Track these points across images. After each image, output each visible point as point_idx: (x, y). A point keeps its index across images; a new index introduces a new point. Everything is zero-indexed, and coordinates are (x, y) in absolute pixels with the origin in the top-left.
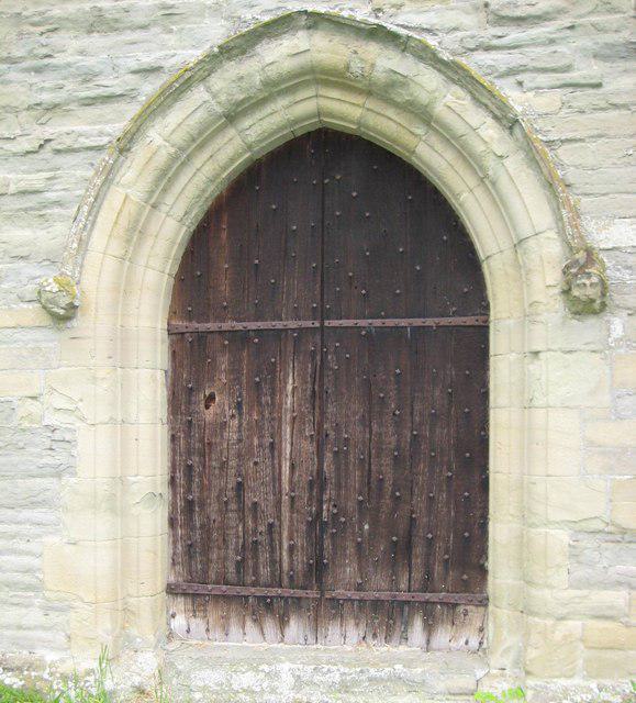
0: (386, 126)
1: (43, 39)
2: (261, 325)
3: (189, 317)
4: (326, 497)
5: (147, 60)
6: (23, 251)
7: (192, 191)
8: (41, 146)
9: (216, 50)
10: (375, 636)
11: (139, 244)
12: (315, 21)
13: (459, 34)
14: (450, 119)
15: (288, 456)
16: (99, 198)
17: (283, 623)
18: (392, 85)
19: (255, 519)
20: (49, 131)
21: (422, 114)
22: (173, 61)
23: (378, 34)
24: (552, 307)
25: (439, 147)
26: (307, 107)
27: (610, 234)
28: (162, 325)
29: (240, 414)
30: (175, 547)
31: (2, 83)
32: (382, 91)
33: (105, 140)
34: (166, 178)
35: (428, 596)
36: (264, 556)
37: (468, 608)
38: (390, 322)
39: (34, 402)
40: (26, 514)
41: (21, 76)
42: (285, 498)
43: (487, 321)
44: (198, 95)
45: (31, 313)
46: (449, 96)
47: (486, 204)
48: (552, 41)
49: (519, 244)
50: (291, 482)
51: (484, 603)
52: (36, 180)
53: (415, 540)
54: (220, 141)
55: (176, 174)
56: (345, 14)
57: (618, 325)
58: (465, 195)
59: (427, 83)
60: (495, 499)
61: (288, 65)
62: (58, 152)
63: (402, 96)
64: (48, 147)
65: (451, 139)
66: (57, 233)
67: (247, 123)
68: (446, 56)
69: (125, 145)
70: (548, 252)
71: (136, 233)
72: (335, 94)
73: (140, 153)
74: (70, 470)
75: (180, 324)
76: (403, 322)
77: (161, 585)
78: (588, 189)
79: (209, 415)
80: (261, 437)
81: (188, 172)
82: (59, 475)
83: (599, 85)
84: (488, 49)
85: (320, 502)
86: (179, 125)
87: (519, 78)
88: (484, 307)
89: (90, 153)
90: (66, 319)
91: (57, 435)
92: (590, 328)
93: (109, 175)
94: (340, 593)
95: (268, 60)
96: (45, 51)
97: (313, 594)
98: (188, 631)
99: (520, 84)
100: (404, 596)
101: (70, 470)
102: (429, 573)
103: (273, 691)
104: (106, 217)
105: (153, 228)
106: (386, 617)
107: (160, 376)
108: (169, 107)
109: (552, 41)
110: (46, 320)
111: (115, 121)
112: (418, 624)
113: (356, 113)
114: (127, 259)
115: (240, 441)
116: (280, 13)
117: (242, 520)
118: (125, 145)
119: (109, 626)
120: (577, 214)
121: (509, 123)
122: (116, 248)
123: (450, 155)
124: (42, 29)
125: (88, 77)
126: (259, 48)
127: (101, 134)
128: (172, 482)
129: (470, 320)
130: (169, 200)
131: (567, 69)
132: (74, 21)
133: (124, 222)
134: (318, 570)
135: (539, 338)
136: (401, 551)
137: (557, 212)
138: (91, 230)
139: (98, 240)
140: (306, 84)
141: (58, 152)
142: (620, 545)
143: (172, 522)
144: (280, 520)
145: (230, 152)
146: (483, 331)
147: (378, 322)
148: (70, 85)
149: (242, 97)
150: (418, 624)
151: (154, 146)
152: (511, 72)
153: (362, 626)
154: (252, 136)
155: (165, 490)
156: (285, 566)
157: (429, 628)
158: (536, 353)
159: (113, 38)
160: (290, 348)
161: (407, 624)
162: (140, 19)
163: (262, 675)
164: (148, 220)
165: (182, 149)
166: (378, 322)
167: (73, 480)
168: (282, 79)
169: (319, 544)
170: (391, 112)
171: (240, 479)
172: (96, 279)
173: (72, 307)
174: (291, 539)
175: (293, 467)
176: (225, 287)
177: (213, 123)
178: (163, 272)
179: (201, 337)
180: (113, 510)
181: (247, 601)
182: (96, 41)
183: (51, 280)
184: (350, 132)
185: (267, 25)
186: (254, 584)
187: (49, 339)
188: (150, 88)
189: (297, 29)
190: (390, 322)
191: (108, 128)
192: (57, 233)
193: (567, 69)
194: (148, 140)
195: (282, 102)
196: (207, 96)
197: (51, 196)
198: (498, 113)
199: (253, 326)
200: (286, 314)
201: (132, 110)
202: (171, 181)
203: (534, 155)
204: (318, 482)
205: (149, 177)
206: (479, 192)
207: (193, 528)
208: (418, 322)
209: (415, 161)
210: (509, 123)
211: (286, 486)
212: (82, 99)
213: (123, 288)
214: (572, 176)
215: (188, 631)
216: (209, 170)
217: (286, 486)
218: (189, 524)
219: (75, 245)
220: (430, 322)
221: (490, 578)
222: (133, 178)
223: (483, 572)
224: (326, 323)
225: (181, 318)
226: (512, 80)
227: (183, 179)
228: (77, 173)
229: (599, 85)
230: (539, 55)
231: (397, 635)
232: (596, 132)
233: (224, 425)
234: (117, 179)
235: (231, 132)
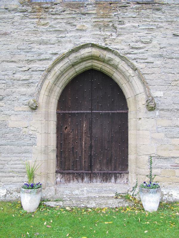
0: (107, 69)
1: (29, 45)
2: (79, 112)
3: (61, 109)
4: (92, 150)
5: (54, 52)
6: (24, 93)
7: (63, 81)
8: (28, 69)
9: (71, 50)
10: (104, 181)
11: (51, 93)
12: (93, 45)
13: (124, 50)
14: (122, 68)
15: (84, 141)
16: (43, 82)
17: (83, 179)
18: (109, 60)
19: (76, 155)
20: (30, 66)
21: (116, 67)
22: (60, 52)
23: (106, 49)
24: (144, 109)
25: (118, 74)
26: (90, 64)
27: (157, 94)
28: (55, 111)
29: (73, 131)
30: (57, 162)
31: (178, 110)
32: (107, 62)
33: (45, 69)
34: (58, 78)
35: (115, 172)
36: (78, 164)
37: (124, 174)
38: (107, 112)
39: (26, 129)
40: (24, 155)
41: (24, 53)
42: (83, 150)
43: (128, 112)
44: (66, 60)
45: (27, 108)
46: (122, 63)
47: (128, 87)
48: (143, 53)
50: (85, 146)
52: (27, 77)
53: (113, 159)
54: (70, 71)
55: (60, 77)
56: (100, 44)
58: (123, 85)
59: (117, 60)
60: (137, 153)
61: (87, 55)
62: (33, 71)
63: (112, 63)
64: (30, 70)
65: (121, 72)
66: (33, 89)
67: (76, 67)
68: (121, 55)
69: (49, 71)
71: (51, 91)
72: (96, 62)
73: (53, 73)
74: (35, 144)
75: (60, 112)
76: (110, 112)
77: (55, 171)
78: (151, 84)
79: (66, 132)
80: (78, 136)
81: (63, 77)
82: (32, 146)
83: (153, 63)
84: (130, 54)
85: (91, 151)
86: (62, 67)
87: (137, 60)
88: (127, 109)
89: (40, 72)
90: (35, 109)
91: (32, 136)
92: (151, 114)
93: (45, 77)
94: (96, 171)
95: (82, 53)
96: (30, 48)
97: (90, 172)
98: (61, 181)
99: (137, 61)
100: (111, 172)
101: (35, 144)
102: (115, 167)
103: (83, 194)
104: (45, 86)
105: (55, 90)
106: (106, 177)
107: (55, 123)
108: (60, 62)
109: (143, 53)
110: (29, 109)
112: (113, 178)
113: (100, 66)
114: (49, 96)
115: (73, 137)
116: (85, 43)
117: (74, 155)
118: (49, 71)
119: (44, 181)
120: (149, 89)
121: (135, 69)
122: (46, 94)
123: (121, 76)
124: (29, 43)
125: (40, 54)
126: (80, 51)
127: (43, 67)
128: (57, 147)
129: (124, 112)
130: (59, 83)
131: (146, 59)
132: (36, 41)
133: (49, 87)
134: (91, 167)
135: (141, 115)
136: (109, 162)
137: (145, 88)
138: (41, 89)
139: (43, 92)
140: (90, 59)
141: (33, 71)
142: (158, 159)
143: (57, 156)
144: (82, 155)
146: (127, 114)
147: (104, 112)
148: (35, 56)
149: (76, 61)
150: (113, 178)
151: (56, 71)
152: (135, 59)
153: (101, 179)
154: (77, 70)
155: (55, 148)
156: (83, 165)
157: (116, 179)
158: (140, 119)
159: (45, 46)
160: (84, 117)
161: (111, 178)
162: (52, 42)
163: (79, 191)
164: (53, 88)
165: (62, 72)
166: (104, 112)
167: (36, 146)
168: (85, 58)
169: (91, 161)
170: (108, 66)
171: (73, 146)
172: (42, 100)
173: (37, 106)
174: (85, 159)
175: (85, 143)
176: (70, 103)
177: (70, 66)
179: (64, 114)
180: (45, 154)
181: (74, 174)
182: (42, 47)
183: (32, 100)
184: (98, 70)
185: (82, 46)
186: (76, 170)
188: (55, 58)
189: (89, 47)
190: (107, 112)
191: (45, 66)
192: (33, 89)
193: (146, 59)
194: (55, 69)
195: (84, 63)
196: (68, 60)
197: (31, 81)
198: (132, 67)
199: (76, 112)
200: (83, 109)
201: (51, 63)
202: (59, 79)
204: (91, 147)
205: (55, 77)
206: (127, 84)
207: (62, 157)
208: (113, 112)
209: (113, 77)
210: (135, 69)
211: (83, 147)
212: (38, 59)
213: (48, 103)
214: (148, 81)
215: (61, 181)
216: (67, 77)
217: (83, 147)
218: (61, 157)
219: (37, 92)
220: (115, 112)
221: (129, 167)
222: (51, 78)
223: (127, 166)
224: (93, 112)
225: (59, 110)
226: (135, 61)
227: (62, 79)
228: (37, 77)
229: (153, 63)
230: (140, 56)
231: (109, 180)
232: (152, 72)
233: (69, 134)
234: (47, 78)
235: (73, 69)
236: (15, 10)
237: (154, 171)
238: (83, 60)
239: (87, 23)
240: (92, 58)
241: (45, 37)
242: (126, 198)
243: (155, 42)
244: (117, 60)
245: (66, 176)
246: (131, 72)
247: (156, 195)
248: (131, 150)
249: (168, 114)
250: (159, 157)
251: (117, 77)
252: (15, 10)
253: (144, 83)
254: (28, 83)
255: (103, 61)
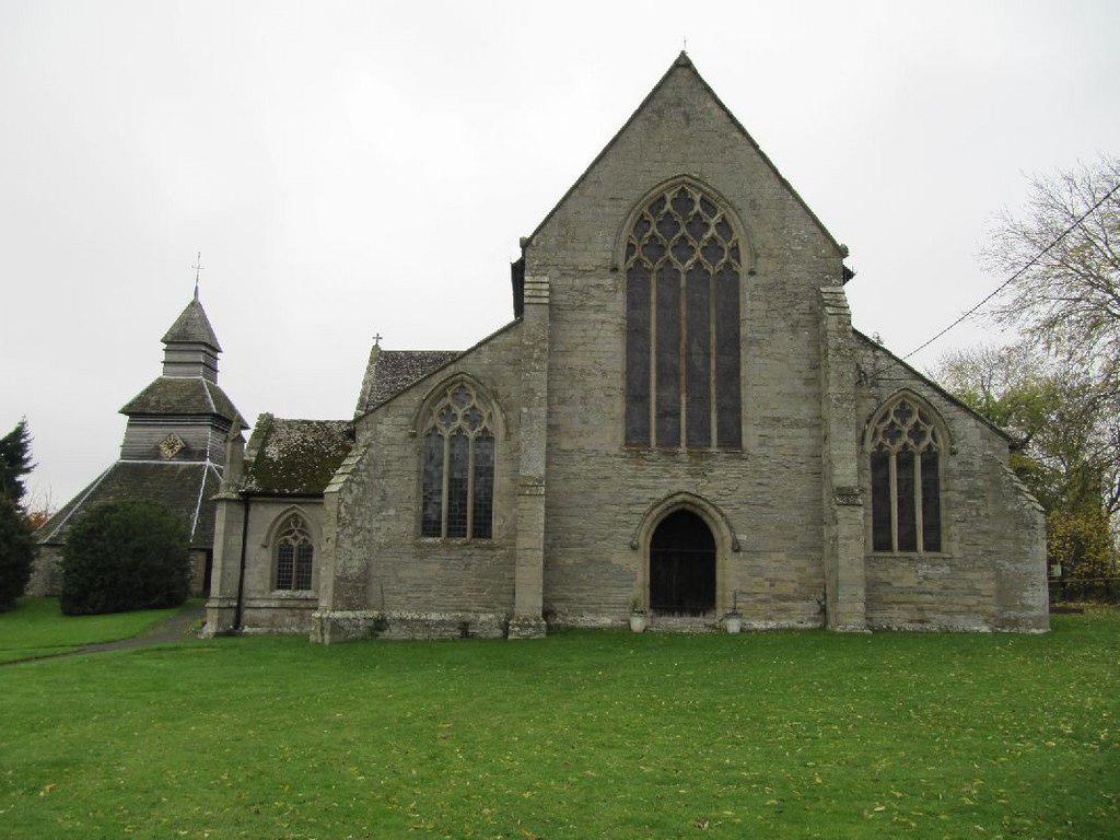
0: (698, 512)
27: (742, 537)
32: (699, 506)
49: (723, 539)
51: (715, 609)
52: (628, 519)
57: (741, 554)
70: (729, 540)
106: (695, 613)
111: (645, 509)
121: (723, 515)
145: (657, 523)
178: (273, 624)
187: (631, 553)
192: (631, 531)
203: (727, 522)
210: (723, 515)
228: (636, 519)
236: (616, 456)
237: (738, 605)
238: (677, 503)
239: (681, 470)
240: (685, 502)
241: (642, 482)
242: (713, 627)
243: (740, 490)
244: (707, 506)
245: (575, 361)
246: (719, 516)
247: (409, 648)
248: (723, 585)
249: (751, 555)
250: (742, 593)
251: (706, 519)
252: (616, 456)
253: (731, 528)
254: (627, 524)
255: (695, 505)
